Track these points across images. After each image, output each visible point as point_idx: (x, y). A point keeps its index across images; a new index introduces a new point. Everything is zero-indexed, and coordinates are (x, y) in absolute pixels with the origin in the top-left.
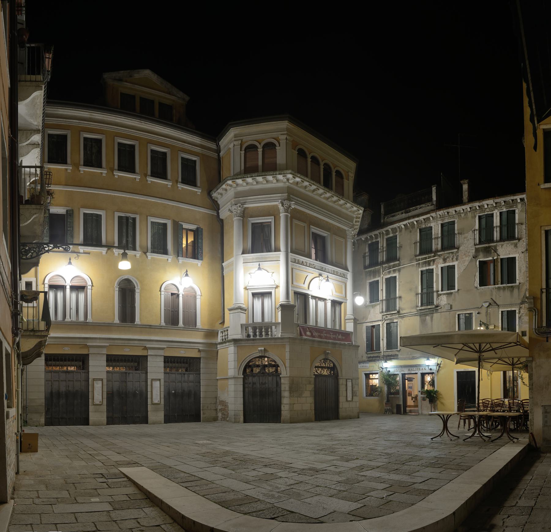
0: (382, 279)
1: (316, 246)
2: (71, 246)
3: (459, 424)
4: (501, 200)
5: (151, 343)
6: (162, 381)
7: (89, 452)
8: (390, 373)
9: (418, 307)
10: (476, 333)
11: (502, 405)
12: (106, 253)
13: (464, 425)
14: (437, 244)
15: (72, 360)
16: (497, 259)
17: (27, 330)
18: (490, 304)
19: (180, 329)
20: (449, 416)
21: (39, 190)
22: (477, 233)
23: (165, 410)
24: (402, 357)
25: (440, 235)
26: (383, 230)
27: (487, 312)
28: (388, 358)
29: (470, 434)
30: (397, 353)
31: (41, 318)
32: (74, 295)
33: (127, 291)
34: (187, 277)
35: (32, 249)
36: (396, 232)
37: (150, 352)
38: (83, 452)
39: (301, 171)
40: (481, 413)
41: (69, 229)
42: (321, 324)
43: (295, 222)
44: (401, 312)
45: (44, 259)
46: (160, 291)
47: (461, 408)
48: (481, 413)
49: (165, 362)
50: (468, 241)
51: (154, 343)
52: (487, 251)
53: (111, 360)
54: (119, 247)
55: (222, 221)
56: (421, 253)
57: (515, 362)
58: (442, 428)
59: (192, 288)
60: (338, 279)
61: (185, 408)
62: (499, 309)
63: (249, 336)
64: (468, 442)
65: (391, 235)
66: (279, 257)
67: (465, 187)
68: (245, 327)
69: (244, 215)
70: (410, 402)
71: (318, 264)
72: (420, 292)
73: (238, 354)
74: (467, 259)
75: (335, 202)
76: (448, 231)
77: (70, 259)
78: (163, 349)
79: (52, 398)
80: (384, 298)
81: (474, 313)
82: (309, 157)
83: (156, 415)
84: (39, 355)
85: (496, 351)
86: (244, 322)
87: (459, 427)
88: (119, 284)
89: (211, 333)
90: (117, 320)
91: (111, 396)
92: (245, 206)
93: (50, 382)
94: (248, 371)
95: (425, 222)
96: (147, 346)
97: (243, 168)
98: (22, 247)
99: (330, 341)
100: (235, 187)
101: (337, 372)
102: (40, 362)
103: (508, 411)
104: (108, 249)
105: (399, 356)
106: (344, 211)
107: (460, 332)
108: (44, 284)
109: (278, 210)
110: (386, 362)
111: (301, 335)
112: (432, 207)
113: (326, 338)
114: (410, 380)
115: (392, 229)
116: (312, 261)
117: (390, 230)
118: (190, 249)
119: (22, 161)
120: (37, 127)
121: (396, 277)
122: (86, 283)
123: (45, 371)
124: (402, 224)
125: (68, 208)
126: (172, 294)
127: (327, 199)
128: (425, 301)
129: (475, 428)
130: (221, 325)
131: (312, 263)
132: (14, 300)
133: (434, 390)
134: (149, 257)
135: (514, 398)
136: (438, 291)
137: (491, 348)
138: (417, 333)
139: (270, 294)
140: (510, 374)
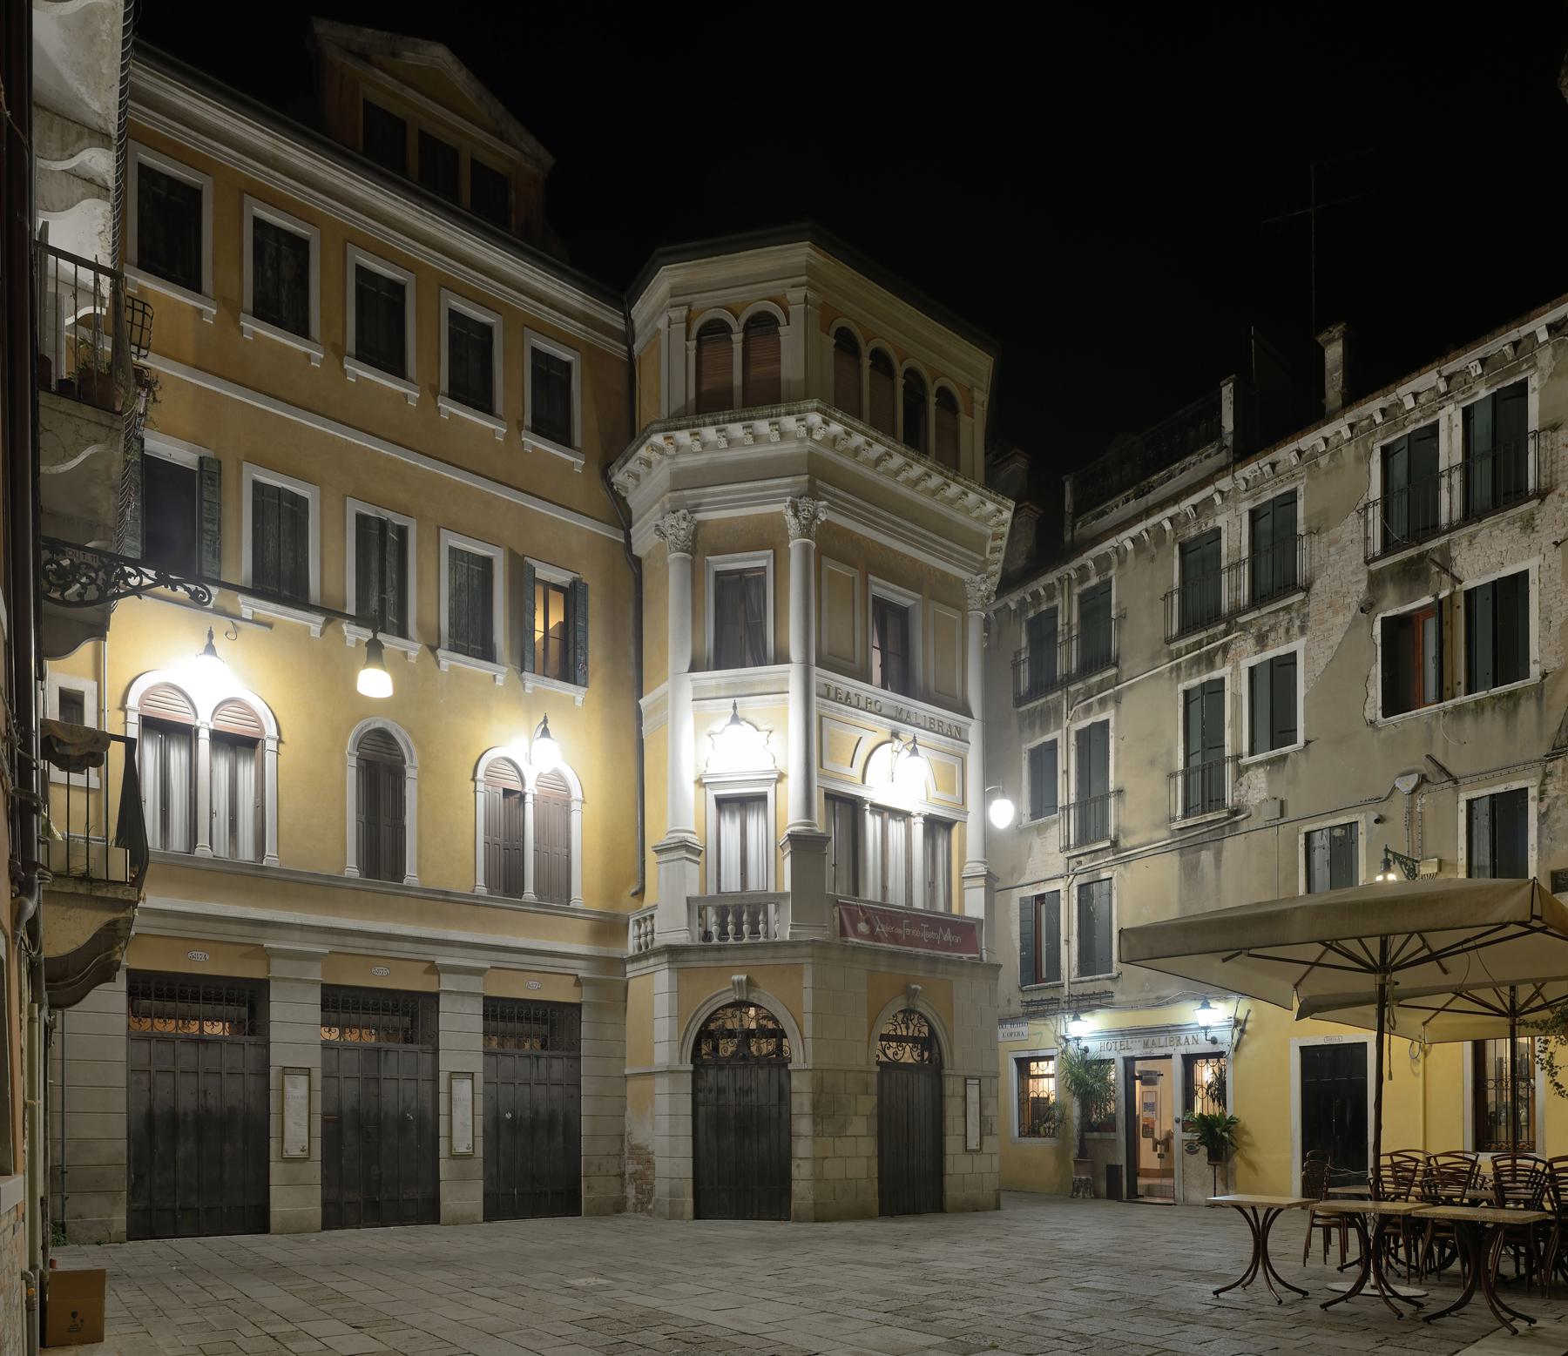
0: (1064, 735)
1: (882, 644)
2: (214, 590)
3: (1308, 1243)
4: (1469, 361)
5: (449, 950)
6: (479, 1078)
7: (268, 1329)
8: (1089, 1056)
9: (1172, 819)
10: (1370, 897)
11: (1465, 1177)
12: (322, 632)
13: (1326, 1251)
14: (1234, 588)
15: (218, 999)
16: (1451, 596)
17: (64, 876)
18: (1423, 779)
19: (528, 909)
20: (1274, 1212)
21: (108, 358)
22: (1375, 514)
23: (488, 1178)
24: (1123, 998)
25: (1245, 554)
26: (1070, 569)
27: (1411, 811)
28: (1083, 1004)
29: (1346, 1287)
30: (1110, 986)
31: (113, 833)
32: (223, 766)
33: (381, 770)
34: (545, 740)
35: (83, 569)
36: (1109, 569)
37: (447, 983)
38: (250, 1331)
39: (844, 402)
40: (1386, 1206)
41: (206, 526)
42: (897, 897)
43: (830, 565)
44: (1123, 843)
45: (126, 614)
46: (474, 779)
47: (1312, 1187)
48: (1386, 1206)
49: (485, 1017)
50: (1340, 557)
51: (457, 951)
52: (1413, 574)
53: (340, 1003)
54: (359, 620)
55: (638, 561)
56: (1184, 631)
57: (1521, 1000)
58: (1250, 1258)
59: (561, 777)
60: (942, 747)
61: (542, 1172)
62: (1456, 791)
63: (707, 936)
64: (1337, 1313)
65: (1094, 581)
66: (786, 681)
67: (1334, 353)
68: (696, 907)
69: (697, 545)
70: (1148, 1157)
71: (889, 698)
72: (1180, 766)
73: (679, 993)
74: (1340, 619)
75: (934, 492)
76: (1275, 530)
77: (211, 635)
78: (479, 972)
79: (154, 1133)
80: (1073, 799)
81: (1364, 820)
82: (866, 351)
83: (462, 1193)
84: (107, 975)
85: (1444, 961)
86: (694, 890)
87: (1306, 1254)
88: (360, 745)
89: (609, 926)
90: (352, 870)
91: (336, 1129)
92: (699, 516)
93: (144, 1077)
94: (705, 1048)
95: (1199, 516)
96: (439, 961)
97: (692, 395)
98: (46, 555)
99: (922, 951)
100: (673, 457)
101: (940, 1054)
102: (111, 998)
103: (1490, 1203)
104: (328, 621)
105: (1117, 998)
106: (960, 518)
107: (1315, 900)
108: (123, 707)
109: (784, 528)
110: (1076, 1018)
111: (843, 933)
112: (1220, 459)
113: (911, 941)
114: (1149, 1079)
115: (1096, 560)
116: (871, 691)
117: (1090, 563)
118: (554, 645)
119: (45, 224)
120: (102, 123)
121: (1106, 722)
122: (261, 727)
123: (128, 1035)
124: (1125, 539)
125: (205, 452)
126: (508, 793)
127: (914, 483)
128: (1196, 798)
129: (1363, 1261)
130: (634, 900)
131: (875, 698)
132: (17, 750)
133: (1223, 1115)
134: (445, 663)
135: (1516, 1151)
136: (1239, 756)
137: (1425, 952)
138: (1170, 913)
139: (761, 799)
140: (1500, 1050)
